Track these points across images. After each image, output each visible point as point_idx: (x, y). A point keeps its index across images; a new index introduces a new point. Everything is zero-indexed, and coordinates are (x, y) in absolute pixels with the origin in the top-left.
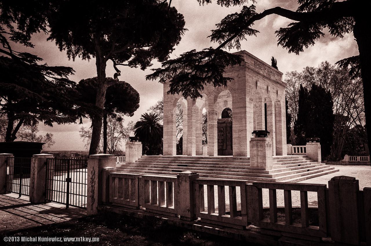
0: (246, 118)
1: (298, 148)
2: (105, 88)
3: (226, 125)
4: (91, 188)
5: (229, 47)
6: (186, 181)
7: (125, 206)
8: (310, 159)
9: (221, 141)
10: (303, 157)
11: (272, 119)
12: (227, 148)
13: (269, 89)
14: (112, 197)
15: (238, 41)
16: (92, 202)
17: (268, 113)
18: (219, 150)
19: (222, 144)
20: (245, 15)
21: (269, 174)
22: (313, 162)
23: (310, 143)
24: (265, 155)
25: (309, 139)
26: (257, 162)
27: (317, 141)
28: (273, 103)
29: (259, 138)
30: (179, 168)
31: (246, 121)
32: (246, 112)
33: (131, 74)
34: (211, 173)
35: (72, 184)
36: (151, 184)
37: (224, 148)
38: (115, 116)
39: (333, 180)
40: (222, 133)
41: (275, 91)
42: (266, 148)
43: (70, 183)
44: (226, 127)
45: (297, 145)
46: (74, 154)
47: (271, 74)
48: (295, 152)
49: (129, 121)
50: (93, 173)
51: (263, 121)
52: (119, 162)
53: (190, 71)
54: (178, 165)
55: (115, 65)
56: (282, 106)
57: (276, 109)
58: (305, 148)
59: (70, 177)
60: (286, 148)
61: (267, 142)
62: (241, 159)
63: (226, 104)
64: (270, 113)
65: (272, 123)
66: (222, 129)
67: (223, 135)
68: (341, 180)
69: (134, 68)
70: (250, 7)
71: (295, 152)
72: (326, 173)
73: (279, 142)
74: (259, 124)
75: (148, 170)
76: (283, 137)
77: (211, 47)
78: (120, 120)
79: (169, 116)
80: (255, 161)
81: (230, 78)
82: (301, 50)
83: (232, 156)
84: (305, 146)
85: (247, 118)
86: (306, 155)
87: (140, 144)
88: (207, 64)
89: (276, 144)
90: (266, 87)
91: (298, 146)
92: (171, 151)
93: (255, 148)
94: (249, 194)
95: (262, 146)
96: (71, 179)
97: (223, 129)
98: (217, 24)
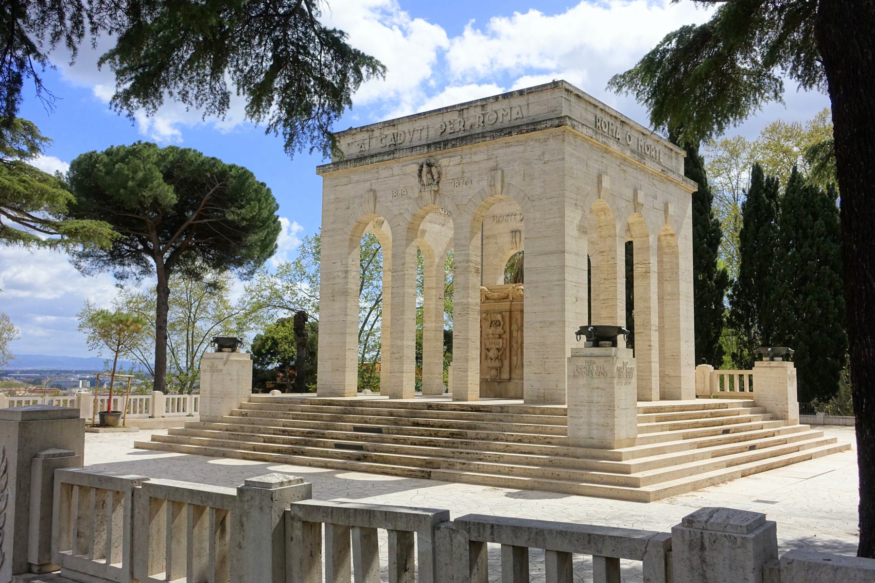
0: (563, 286)
1: (731, 377)
3: (511, 305)
8: (764, 411)
9: (496, 352)
10: (745, 405)
11: (648, 290)
12: (514, 376)
13: (641, 198)
14: (59, 549)
17: (637, 270)
18: (484, 382)
19: (497, 364)
21: (623, 462)
22: (772, 419)
23: (766, 361)
24: (613, 401)
25: (762, 352)
26: (589, 424)
27: (786, 358)
28: (652, 239)
29: (596, 351)
30: (357, 438)
31: (563, 295)
32: (563, 267)
36: (377, 467)
37: (505, 376)
39: (686, 524)
40: (499, 330)
41: (659, 204)
42: (616, 380)
44: (510, 312)
46: (88, 379)
47: (648, 153)
48: (724, 388)
51: (619, 297)
52: (193, 413)
54: (356, 429)
56: (680, 250)
57: (665, 259)
58: (750, 376)
60: (693, 375)
61: (619, 364)
62: (543, 412)
63: (518, 240)
64: (644, 270)
65: (647, 300)
66: (499, 317)
68: (713, 523)
71: (722, 389)
72: (807, 455)
73: (669, 359)
75: (264, 442)
76: (682, 343)
79: (336, 274)
80: (582, 420)
83: (522, 402)
84: (749, 372)
85: (568, 285)
86: (751, 398)
87: (245, 361)
90: (629, 194)
92: (342, 383)
93: (582, 381)
95: (603, 374)
97: (503, 317)
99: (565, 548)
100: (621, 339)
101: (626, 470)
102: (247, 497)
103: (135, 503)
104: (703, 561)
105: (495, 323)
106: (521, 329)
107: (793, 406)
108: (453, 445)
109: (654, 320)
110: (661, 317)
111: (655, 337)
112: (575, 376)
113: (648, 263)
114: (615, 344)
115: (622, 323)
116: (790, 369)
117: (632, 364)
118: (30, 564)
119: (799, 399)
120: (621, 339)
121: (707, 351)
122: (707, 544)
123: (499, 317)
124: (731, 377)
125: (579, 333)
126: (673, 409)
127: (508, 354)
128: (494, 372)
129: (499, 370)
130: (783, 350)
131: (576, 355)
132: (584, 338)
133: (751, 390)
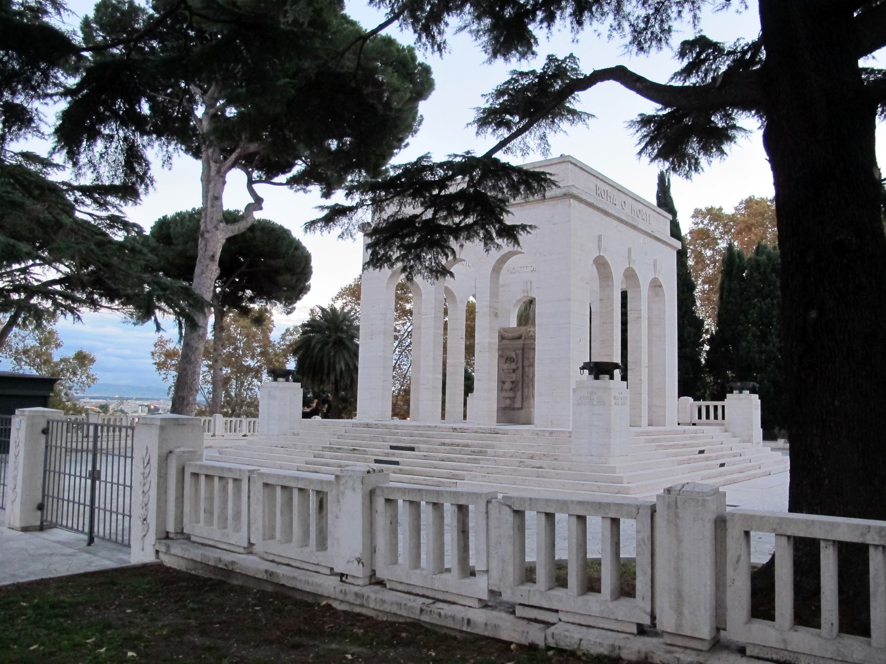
1: (708, 408)
2: (215, 241)
4: (141, 497)
5: (522, 150)
6: (354, 489)
7: (218, 545)
11: (639, 333)
15: (543, 137)
16: (143, 530)
19: (511, 394)
20: (555, 76)
27: (753, 391)
33: (288, 205)
34: (474, 469)
35: (103, 484)
38: (245, 312)
40: (514, 366)
43: (97, 482)
44: (523, 349)
45: (712, 400)
49: (285, 321)
50: (146, 461)
52: (248, 434)
53: (419, 210)
55: (251, 182)
58: (723, 407)
59: (98, 468)
67: (514, 371)
69: (301, 193)
70: (566, 58)
71: (700, 417)
73: (656, 392)
74: (607, 342)
77: (468, 152)
78: (260, 320)
81: (526, 226)
82: (696, 166)
88: (461, 195)
89: (650, 397)
91: (716, 403)
94: (493, 523)
96: (99, 472)
97: (517, 355)
98: (486, 95)
99: (581, 513)
100: (617, 373)
101: (619, 480)
102: (342, 481)
103: (251, 488)
104: (677, 516)
105: (509, 360)
106: (533, 365)
107: (758, 432)
108: (476, 461)
109: (645, 359)
110: (650, 356)
111: (645, 372)
112: (579, 404)
113: (640, 306)
114: (612, 378)
115: (618, 360)
116: (755, 399)
117: (627, 393)
118: (168, 533)
119: (763, 425)
120: (617, 373)
121: (689, 385)
122: (679, 504)
123: (513, 355)
124: (708, 408)
125: (583, 368)
126: (659, 433)
127: (520, 387)
128: (508, 402)
129: (513, 399)
130: (751, 384)
131: (580, 385)
132: (586, 371)
133: (723, 418)
